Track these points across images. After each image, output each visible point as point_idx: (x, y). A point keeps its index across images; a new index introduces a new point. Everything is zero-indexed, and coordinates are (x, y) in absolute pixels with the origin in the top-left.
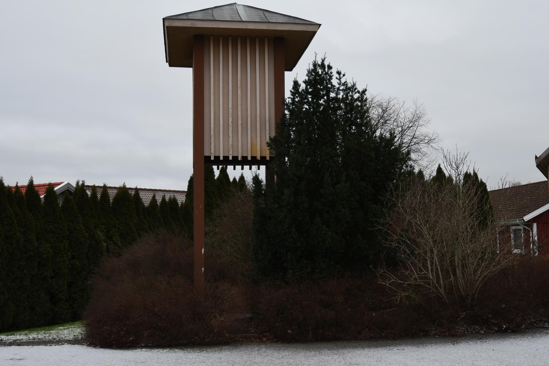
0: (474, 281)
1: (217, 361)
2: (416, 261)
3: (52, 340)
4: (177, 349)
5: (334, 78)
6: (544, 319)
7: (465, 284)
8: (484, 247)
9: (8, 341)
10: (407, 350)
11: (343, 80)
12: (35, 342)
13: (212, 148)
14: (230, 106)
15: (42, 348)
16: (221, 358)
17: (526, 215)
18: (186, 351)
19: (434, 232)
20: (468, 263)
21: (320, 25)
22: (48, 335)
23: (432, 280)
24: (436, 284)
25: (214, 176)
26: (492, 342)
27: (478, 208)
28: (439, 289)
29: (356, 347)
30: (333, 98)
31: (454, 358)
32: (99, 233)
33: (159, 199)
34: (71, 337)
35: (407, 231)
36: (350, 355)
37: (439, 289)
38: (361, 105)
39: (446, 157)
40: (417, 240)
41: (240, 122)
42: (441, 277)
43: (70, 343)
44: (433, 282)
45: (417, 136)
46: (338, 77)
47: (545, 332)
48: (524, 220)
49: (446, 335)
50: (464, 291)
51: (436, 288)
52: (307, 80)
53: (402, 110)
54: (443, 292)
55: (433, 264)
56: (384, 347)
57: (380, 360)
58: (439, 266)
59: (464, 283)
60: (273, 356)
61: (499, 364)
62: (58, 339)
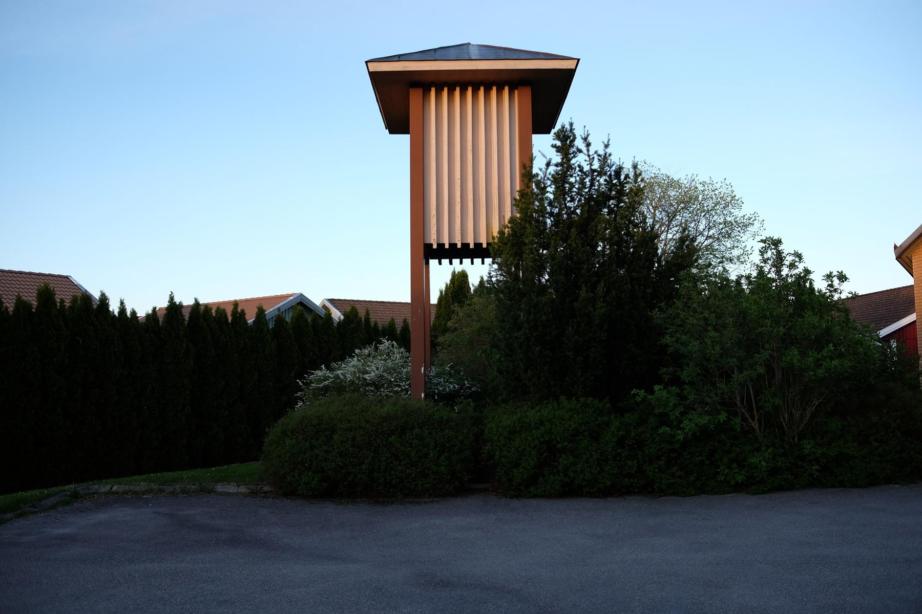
28: (750, 420)
37: (750, 420)
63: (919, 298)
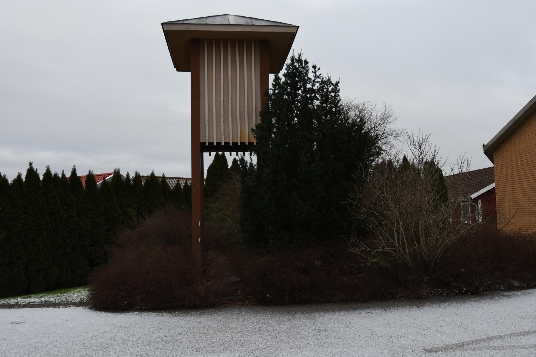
0: (436, 249)
1: (195, 325)
2: (384, 231)
3: (61, 302)
4: (166, 312)
5: (310, 71)
6: (499, 281)
7: (428, 251)
8: (445, 218)
9: (23, 303)
10: (375, 314)
11: (318, 73)
12: (46, 304)
13: (207, 135)
14: (222, 100)
15: (51, 310)
16: (200, 323)
17: (473, 194)
18: (173, 314)
19: (400, 206)
20: (431, 232)
21: (298, 27)
22: (58, 298)
23: (398, 248)
24: (402, 251)
25: (228, 165)
26: (454, 305)
27: (439, 183)
29: (328, 311)
30: (309, 89)
31: (419, 324)
32: (131, 210)
33: (182, 183)
34: (78, 300)
35: (375, 204)
36: (321, 320)
38: (335, 95)
39: (410, 138)
40: (385, 212)
41: (230, 113)
42: (406, 245)
43: (75, 305)
44: (399, 249)
45: (386, 131)
46: (314, 71)
47: (502, 294)
48: (471, 198)
49: (411, 298)
50: (427, 257)
51: (402, 255)
52: (286, 73)
53: (374, 111)
54: (408, 259)
55: (399, 233)
56: (354, 311)
57: (348, 325)
58: (404, 236)
59: (427, 250)
60: (249, 321)
61: (463, 330)
62: (66, 302)
63: (496, 176)
